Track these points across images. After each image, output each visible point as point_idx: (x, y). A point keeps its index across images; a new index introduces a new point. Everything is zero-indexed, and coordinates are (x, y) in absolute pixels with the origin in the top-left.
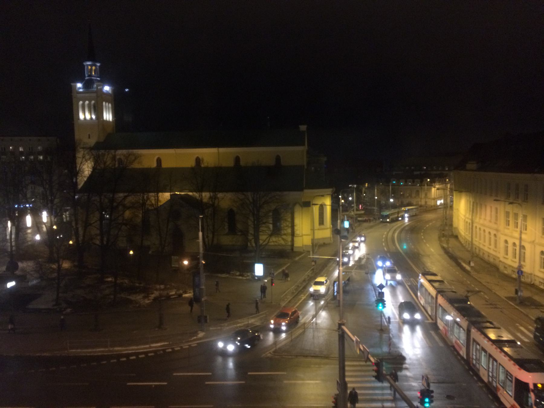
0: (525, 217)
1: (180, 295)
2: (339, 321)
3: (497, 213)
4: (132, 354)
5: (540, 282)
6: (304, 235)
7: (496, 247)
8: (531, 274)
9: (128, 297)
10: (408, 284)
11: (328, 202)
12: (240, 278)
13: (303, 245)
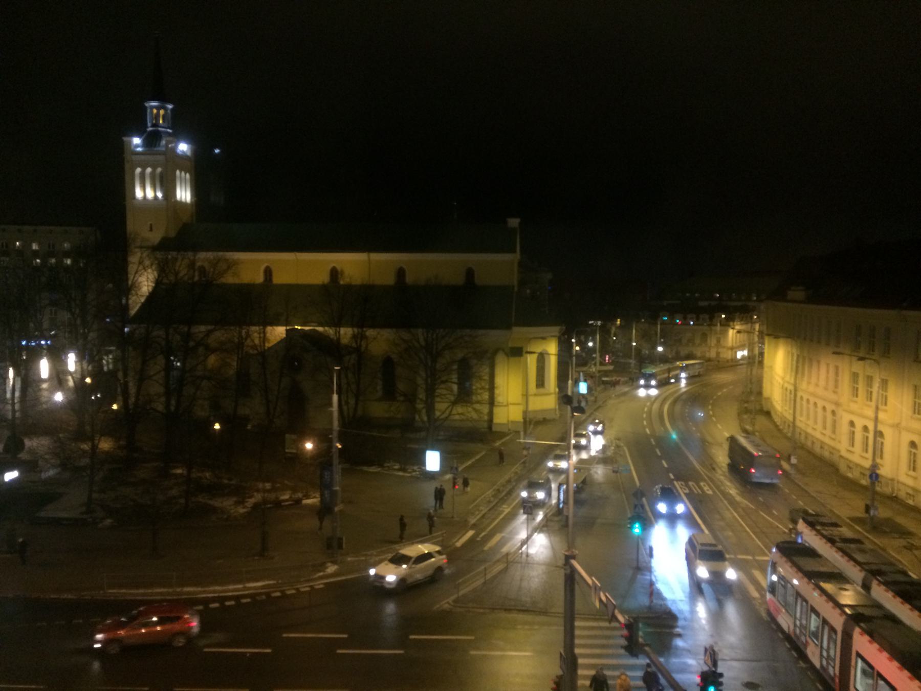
0: (884, 383)
1: (298, 502)
2: (566, 551)
3: (837, 374)
4: (214, 600)
5: (908, 494)
6: (511, 404)
7: (834, 432)
8: (892, 480)
9: (211, 502)
10: (685, 492)
11: (552, 348)
12: (401, 473)
13: (508, 421)
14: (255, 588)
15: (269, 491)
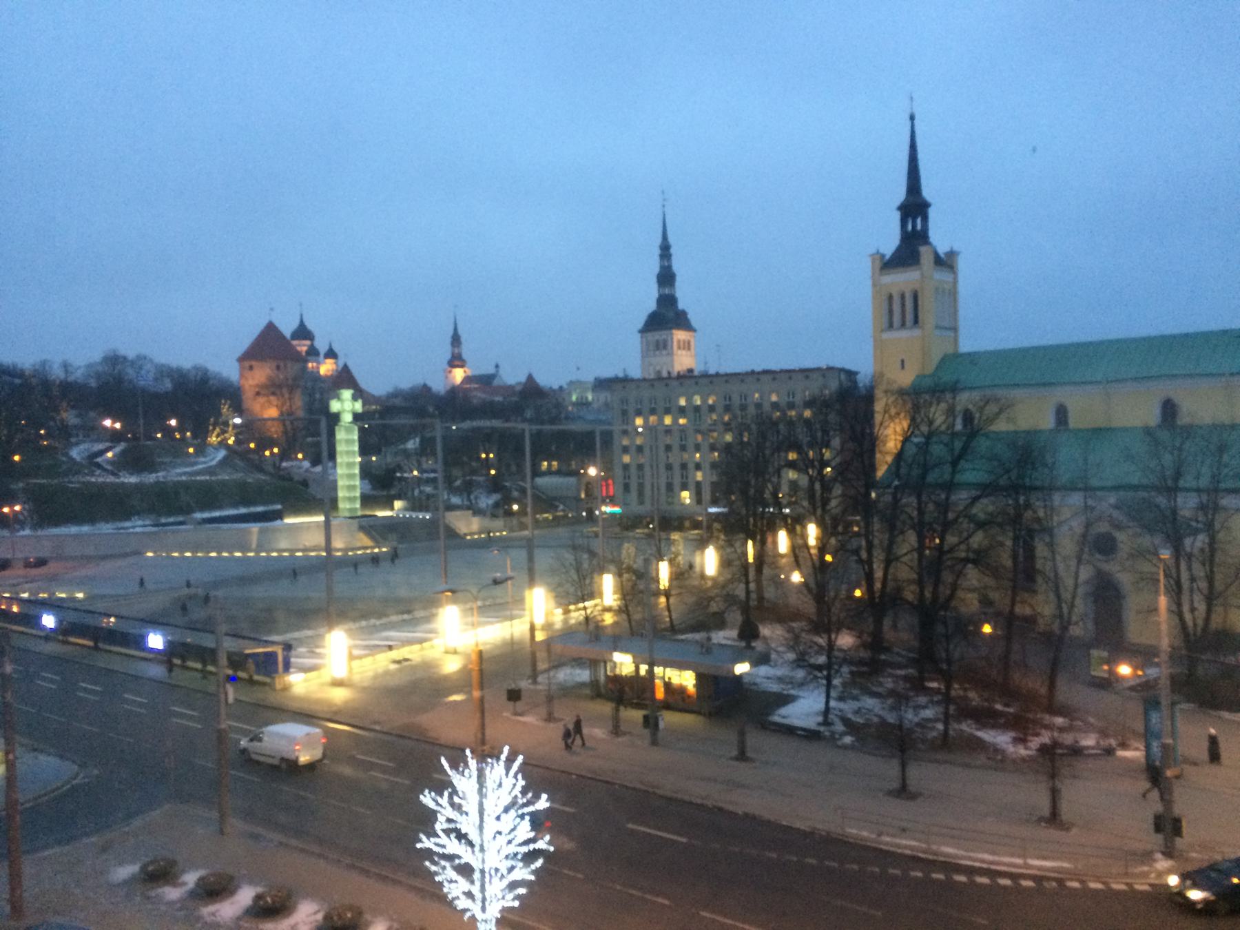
1: (1109, 752)
9: (980, 734)
12: (301, 487)
14: (1040, 868)
15: (1061, 730)
